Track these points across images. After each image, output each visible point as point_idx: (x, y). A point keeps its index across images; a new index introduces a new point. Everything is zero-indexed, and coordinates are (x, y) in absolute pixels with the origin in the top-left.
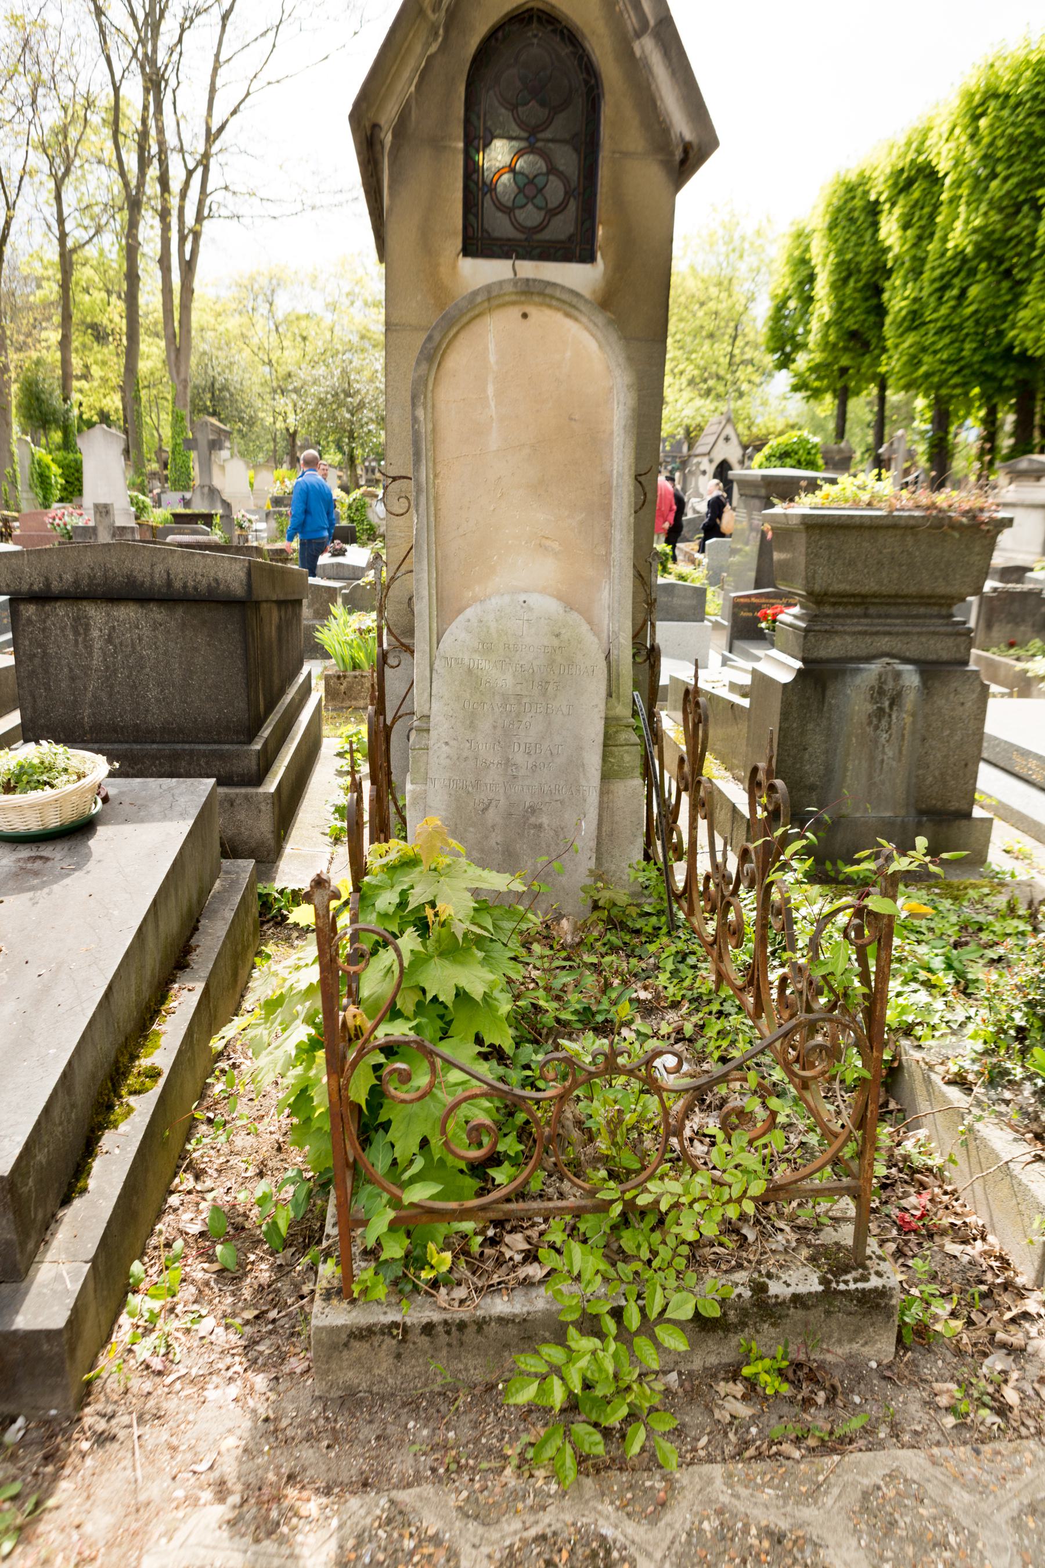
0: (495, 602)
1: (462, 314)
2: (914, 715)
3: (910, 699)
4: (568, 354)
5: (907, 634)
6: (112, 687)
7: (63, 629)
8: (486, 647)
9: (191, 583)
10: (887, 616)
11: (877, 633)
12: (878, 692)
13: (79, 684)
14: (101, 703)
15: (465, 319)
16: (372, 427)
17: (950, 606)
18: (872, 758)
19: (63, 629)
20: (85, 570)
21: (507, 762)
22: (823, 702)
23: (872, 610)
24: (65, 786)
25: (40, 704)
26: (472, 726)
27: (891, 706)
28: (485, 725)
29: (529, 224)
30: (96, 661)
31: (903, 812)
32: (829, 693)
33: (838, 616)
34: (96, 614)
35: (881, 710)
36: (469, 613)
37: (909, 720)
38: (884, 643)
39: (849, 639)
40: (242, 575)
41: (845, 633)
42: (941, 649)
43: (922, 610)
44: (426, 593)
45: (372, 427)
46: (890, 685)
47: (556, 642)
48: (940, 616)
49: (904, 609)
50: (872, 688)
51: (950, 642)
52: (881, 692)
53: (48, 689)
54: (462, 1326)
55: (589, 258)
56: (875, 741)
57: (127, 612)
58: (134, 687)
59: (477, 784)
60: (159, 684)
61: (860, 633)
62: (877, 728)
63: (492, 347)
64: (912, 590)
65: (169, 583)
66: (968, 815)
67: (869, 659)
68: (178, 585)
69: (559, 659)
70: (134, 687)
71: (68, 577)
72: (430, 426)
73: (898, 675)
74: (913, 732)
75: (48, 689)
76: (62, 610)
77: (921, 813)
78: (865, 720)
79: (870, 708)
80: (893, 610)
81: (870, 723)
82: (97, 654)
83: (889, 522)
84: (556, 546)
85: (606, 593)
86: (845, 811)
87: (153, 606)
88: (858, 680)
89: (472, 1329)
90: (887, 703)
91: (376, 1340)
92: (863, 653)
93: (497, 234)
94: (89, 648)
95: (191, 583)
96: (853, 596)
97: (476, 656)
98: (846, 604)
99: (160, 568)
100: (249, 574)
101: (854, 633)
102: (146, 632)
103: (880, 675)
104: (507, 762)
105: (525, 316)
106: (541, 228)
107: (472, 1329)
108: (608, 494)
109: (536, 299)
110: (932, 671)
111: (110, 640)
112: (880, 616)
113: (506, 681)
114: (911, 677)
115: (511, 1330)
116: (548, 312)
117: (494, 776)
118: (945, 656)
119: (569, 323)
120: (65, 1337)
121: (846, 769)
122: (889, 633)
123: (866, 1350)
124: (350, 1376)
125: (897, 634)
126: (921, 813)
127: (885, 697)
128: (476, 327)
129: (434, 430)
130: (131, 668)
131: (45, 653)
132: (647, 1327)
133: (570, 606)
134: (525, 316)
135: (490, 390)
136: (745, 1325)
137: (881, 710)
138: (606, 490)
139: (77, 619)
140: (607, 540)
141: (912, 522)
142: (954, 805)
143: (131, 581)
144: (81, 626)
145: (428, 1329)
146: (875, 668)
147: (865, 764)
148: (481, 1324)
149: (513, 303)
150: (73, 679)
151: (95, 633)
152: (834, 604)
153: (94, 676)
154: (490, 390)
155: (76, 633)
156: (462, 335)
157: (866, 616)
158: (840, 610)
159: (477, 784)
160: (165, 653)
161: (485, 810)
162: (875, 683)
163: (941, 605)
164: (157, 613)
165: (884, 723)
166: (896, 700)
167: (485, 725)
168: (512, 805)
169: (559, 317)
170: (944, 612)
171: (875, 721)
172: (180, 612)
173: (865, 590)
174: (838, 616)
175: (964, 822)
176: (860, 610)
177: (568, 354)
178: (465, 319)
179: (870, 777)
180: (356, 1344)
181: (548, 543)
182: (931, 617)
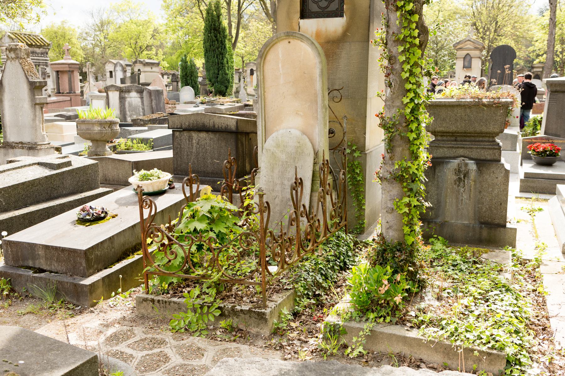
0: (281, 132)
1: (270, 44)
2: (475, 181)
3: (473, 175)
4: (303, 53)
5: (472, 148)
6: (198, 158)
7: (186, 140)
8: (278, 146)
9: (220, 126)
10: (465, 141)
11: (458, 148)
12: (458, 171)
13: (189, 157)
14: (195, 164)
15: (271, 45)
16: (446, 58)
17: (493, 137)
18: (457, 198)
19: (186, 140)
20: (191, 122)
21: (282, 184)
22: (435, 174)
23: (458, 139)
24: (155, 180)
25: (179, 163)
26: (273, 171)
27: (464, 177)
28: (276, 171)
29: (323, 6)
30: (194, 150)
31: (473, 222)
32: (437, 171)
33: (443, 141)
34: (194, 135)
35: (460, 178)
36: (274, 135)
37: (473, 183)
38: (461, 152)
39: (446, 150)
40: (235, 123)
41: (444, 147)
42: (487, 154)
43: (481, 139)
44: (261, 128)
45: (446, 58)
46: (463, 169)
47: (298, 145)
48: (489, 141)
49: (473, 139)
50: (455, 169)
51: (491, 152)
52: (459, 171)
53: (181, 158)
54: (166, 302)
55: (342, 16)
56: (458, 191)
57: (203, 135)
58: (204, 159)
59: (273, 190)
60: (211, 158)
61: (450, 147)
62: (458, 186)
63: (280, 52)
64: (472, 130)
65: (214, 126)
66: (504, 226)
67: (455, 158)
68: (216, 126)
69: (299, 150)
70: (204, 159)
71: (187, 124)
72: (262, 77)
73: (466, 165)
74: (475, 189)
75: (181, 158)
76: (186, 134)
77: (482, 223)
78: (453, 183)
79: (455, 177)
80: (467, 139)
81: (455, 184)
82: (194, 147)
83: (457, 104)
84: (301, 113)
85: (317, 129)
86: (447, 219)
87: (210, 133)
88: (449, 166)
89: (168, 303)
90: (462, 176)
91: (148, 302)
92: (452, 155)
93: (313, 11)
94: (192, 146)
95: (220, 126)
96: (447, 132)
97: (275, 149)
98: (447, 136)
99: (212, 121)
100: (237, 123)
101: (448, 147)
102: (208, 141)
103: (459, 164)
104: (282, 184)
105: (289, 42)
106: (327, 7)
107: (168, 303)
108: (316, 97)
109: (291, 37)
110: (481, 163)
111: (198, 144)
112: (461, 141)
113: (283, 157)
114: (472, 166)
115: (176, 305)
116: (296, 41)
117: (278, 188)
118: (489, 158)
119: (302, 43)
120: (88, 287)
121: (446, 202)
122: (463, 148)
123: (261, 331)
124: (143, 311)
125: (467, 148)
126: (482, 223)
127: (462, 175)
128: (275, 47)
129: (264, 78)
130: (203, 153)
131: (181, 147)
132: (208, 313)
133: (304, 133)
134: (289, 42)
135: (280, 65)
136: (230, 316)
137: (460, 179)
138: (316, 95)
139: (189, 137)
140: (317, 110)
141: (467, 103)
142: (497, 221)
143: (204, 125)
144: (190, 139)
145: (159, 301)
146: (456, 161)
147: (454, 201)
148: (170, 302)
149: (286, 39)
150: (188, 155)
151: (194, 141)
152: (442, 136)
153: (193, 155)
154: (280, 65)
155: (189, 141)
156: (271, 49)
157: (456, 141)
158: (445, 138)
159: (273, 190)
160: (213, 148)
161: (275, 199)
162: (457, 168)
163: (489, 137)
164: (211, 135)
165: (462, 184)
166: (466, 175)
167: (276, 171)
168: (283, 198)
169: (299, 42)
170: (491, 139)
171: (457, 183)
172: (218, 135)
173: (451, 130)
174: (443, 141)
175: (502, 229)
176: (453, 138)
177: (303, 53)
178: (271, 45)
179: (457, 206)
180: (144, 302)
181: (299, 113)
182: (485, 141)
